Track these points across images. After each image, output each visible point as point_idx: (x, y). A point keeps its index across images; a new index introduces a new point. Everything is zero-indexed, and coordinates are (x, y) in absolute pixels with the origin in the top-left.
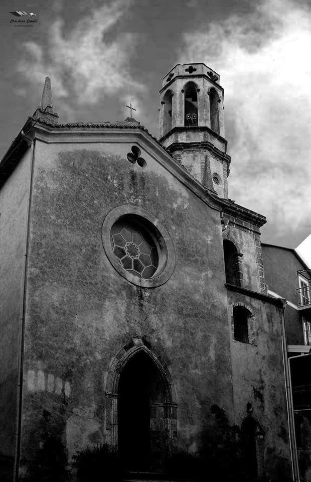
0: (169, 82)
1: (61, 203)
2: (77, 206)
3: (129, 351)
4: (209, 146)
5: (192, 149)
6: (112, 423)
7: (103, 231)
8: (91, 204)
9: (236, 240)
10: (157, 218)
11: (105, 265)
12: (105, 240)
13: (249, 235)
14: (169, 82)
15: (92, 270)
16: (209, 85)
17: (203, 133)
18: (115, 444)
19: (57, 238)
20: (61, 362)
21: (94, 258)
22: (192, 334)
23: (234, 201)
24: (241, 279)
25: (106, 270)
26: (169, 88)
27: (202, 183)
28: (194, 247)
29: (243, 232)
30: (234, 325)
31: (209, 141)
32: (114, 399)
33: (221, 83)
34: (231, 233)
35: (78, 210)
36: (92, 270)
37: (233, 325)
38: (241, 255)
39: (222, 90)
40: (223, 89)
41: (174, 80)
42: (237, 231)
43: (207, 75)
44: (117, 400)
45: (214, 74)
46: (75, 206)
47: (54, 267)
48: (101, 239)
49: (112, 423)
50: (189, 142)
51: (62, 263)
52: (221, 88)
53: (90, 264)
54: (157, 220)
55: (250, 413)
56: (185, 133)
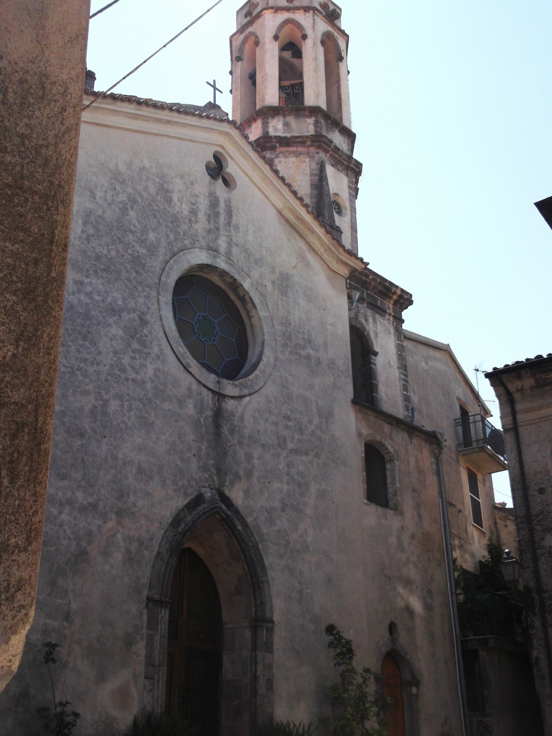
0: (249, 18)
1: (91, 230)
2: (118, 238)
3: (194, 513)
4: (324, 143)
5: (294, 149)
6: (157, 664)
7: (160, 290)
8: (142, 238)
9: (367, 328)
10: (250, 277)
11: (161, 350)
12: (162, 304)
13: (386, 322)
14: (249, 18)
15: (138, 356)
16: (323, 26)
17: (314, 118)
18: (159, 711)
19: (79, 291)
20: (68, 531)
21: (143, 334)
22: (299, 485)
23: (368, 264)
24: (374, 394)
25: (162, 357)
26: (251, 29)
27: (456, 577)
28: (306, 332)
29: (377, 316)
30: (366, 473)
31: (324, 133)
32: (163, 611)
33: (345, 23)
34: (360, 315)
35: (120, 247)
36: (138, 356)
37: (365, 474)
38: (376, 354)
39: (346, 36)
40: (347, 36)
41: (259, 16)
42: (369, 313)
43: (319, 8)
44: (168, 612)
45: (331, 7)
46: (59, 238)
47: (70, 343)
48: (156, 303)
49: (157, 664)
50: (289, 135)
51: (85, 338)
52: (343, 33)
53: (135, 346)
54: (248, 280)
55: (394, 641)
56: (281, 118)
